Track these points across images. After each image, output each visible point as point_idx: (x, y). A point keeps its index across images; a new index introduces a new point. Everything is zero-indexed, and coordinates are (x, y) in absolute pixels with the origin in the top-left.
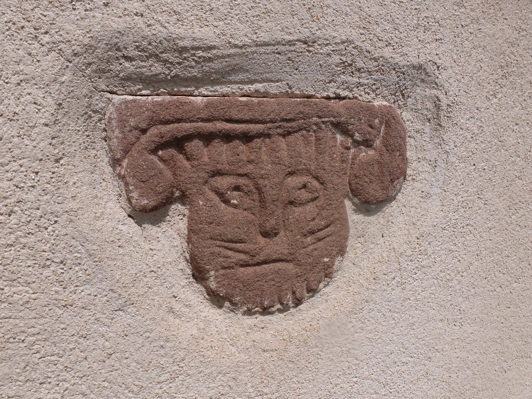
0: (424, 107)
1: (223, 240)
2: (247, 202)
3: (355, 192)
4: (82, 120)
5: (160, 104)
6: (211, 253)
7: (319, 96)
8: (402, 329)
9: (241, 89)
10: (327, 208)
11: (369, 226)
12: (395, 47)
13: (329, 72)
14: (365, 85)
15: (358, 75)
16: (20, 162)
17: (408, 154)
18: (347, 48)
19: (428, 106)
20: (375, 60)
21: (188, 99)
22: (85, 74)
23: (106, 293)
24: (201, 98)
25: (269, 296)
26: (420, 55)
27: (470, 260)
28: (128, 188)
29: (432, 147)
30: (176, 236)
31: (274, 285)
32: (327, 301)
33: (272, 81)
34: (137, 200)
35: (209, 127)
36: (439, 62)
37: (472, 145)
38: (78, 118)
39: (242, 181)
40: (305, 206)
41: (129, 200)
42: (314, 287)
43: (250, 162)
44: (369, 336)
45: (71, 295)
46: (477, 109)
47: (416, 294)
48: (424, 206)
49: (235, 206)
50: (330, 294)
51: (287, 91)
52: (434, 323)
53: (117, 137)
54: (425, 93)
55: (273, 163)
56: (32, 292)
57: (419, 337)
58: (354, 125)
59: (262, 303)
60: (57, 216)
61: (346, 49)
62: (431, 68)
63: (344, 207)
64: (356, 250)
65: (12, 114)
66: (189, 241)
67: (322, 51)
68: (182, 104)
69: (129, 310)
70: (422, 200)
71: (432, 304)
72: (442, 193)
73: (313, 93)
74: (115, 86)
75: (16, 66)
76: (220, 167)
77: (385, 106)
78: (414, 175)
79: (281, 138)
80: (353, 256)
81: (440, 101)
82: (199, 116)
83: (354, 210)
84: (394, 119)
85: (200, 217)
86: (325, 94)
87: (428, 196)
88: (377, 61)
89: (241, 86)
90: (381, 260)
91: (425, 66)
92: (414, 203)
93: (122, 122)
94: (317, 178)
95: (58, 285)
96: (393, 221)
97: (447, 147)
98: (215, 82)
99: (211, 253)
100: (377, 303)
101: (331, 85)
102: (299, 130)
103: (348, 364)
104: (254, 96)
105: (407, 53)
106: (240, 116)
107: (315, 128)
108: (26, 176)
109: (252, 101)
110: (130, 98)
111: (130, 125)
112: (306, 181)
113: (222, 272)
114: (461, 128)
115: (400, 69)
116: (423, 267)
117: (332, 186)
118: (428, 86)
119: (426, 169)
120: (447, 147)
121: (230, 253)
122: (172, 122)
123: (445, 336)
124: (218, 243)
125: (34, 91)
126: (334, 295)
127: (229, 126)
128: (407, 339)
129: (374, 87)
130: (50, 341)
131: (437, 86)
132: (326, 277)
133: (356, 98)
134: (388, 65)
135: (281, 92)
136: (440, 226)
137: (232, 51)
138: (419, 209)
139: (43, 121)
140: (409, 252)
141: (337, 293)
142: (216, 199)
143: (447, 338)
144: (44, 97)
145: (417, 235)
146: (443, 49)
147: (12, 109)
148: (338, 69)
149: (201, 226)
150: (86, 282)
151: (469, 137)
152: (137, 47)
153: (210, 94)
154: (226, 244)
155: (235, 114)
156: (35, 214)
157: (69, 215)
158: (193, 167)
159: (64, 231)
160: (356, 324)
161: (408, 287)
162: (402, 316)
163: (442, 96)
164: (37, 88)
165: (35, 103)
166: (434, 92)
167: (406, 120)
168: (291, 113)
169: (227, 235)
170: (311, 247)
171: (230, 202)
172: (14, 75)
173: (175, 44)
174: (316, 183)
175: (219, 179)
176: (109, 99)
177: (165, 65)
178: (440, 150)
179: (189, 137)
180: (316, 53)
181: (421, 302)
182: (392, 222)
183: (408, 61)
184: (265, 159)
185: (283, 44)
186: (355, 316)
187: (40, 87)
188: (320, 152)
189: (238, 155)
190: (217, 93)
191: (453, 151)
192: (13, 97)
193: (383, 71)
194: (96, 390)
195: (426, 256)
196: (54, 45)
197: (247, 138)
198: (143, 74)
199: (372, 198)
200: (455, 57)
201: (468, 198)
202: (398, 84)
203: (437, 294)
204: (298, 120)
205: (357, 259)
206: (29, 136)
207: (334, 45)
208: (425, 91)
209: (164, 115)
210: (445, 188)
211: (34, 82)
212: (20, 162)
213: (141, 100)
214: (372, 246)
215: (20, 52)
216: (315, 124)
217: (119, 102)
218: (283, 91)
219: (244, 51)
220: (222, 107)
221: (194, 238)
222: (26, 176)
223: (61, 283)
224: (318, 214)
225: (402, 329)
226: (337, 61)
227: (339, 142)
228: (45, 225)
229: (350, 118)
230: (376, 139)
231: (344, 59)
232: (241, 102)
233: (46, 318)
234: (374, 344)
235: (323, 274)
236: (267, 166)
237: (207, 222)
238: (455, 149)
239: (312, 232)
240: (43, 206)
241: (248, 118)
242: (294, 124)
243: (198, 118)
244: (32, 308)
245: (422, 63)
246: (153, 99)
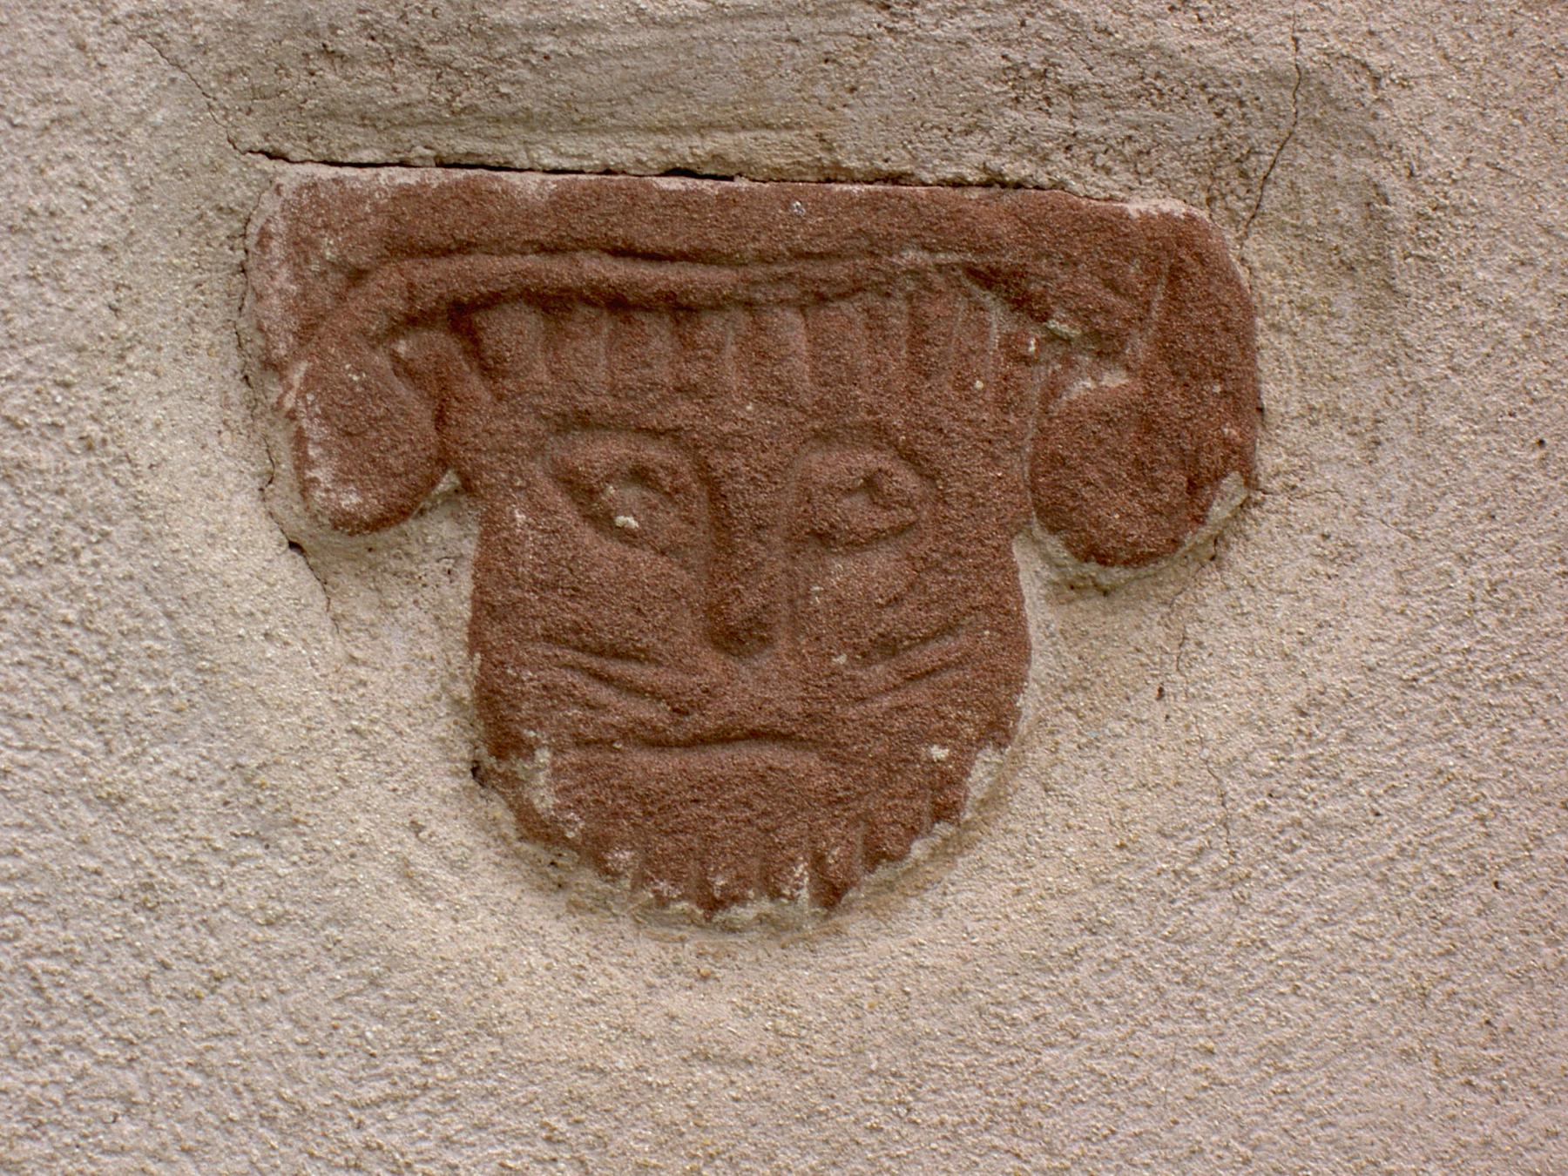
0: (1328, 221)
1: (584, 648)
2: (669, 519)
3: (1055, 517)
4: (190, 236)
5: (406, 193)
6: (545, 687)
7: (926, 176)
8: (1238, 1062)
9: (666, 152)
10: (947, 565)
11: (1109, 652)
12: (1203, 14)
13: (963, 100)
14: (1097, 141)
15: (1069, 108)
16: (29, 353)
17: (1270, 392)
18: (1029, 21)
19: (1344, 217)
20: (1132, 58)
21: (499, 180)
22: (214, 103)
23: (222, 776)
24: (539, 177)
25: (731, 859)
26: (1303, 37)
27: (1532, 823)
28: (305, 453)
29: (1364, 368)
30: (427, 626)
31: (749, 822)
32: (939, 912)
33: (768, 126)
34: (327, 491)
35: (559, 271)
36: (1376, 60)
37: (1529, 368)
38: (180, 231)
39: (655, 453)
40: (869, 554)
41: (305, 488)
42: (889, 846)
43: (686, 390)
44: (1103, 1066)
45: (125, 767)
46: (1548, 231)
47: (1294, 930)
48: (1328, 591)
49: (626, 536)
50: (952, 889)
51: (819, 160)
52: (1376, 1059)
53: (280, 291)
54: (1333, 171)
55: (763, 397)
56: (21, 744)
57: (1310, 1105)
58: (1048, 276)
59: (705, 885)
60: (108, 520)
61: (1023, 24)
62: (1345, 83)
63: (1010, 571)
64: (1058, 738)
65: (20, 215)
66: (476, 641)
67: (939, 32)
68: (475, 193)
69: (285, 842)
70: (1320, 568)
71: (1364, 981)
72: (1403, 546)
73: (907, 168)
74: (288, 137)
75: (44, 80)
76: (587, 402)
77: (1167, 217)
78: (1294, 473)
79: (791, 316)
80: (1042, 754)
81: (1387, 202)
82: (532, 236)
83: (1046, 597)
84: (1202, 262)
85: (515, 565)
86: (949, 172)
87: (1347, 554)
88: (1134, 62)
89: (665, 141)
90: (1152, 780)
91: (1324, 78)
92: (1289, 575)
93: (301, 246)
94: (909, 457)
95: (91, 732)
96: (1203, 638)
97: (1421, 373)
98: (579, 127)
99: (545, 687)
100: (1132, 941)
101: (972, 141)
102: (854, 291)
103: (1016, 1163)
104: (707, 171)
105: (1252, 31)
106: (660, 240)
107: (911, 286)
108: (38, 392)
109: (701, 192)
110: (327, 172)
111: (322, 257)
112: (873, 466)
113: (574, 756)
114: (1479, 302)
115: (1225, 85)
116: (1324, 824)
117: (965, 490)
118: (1342, 143)
119: (1341, 451)
120: (1421, 373)
121: (604, 694)
122: (447, 252)
123: (1425, 1125)
124: (570, 656)
125: (82, 151)
126: (970, 895)
127: (617, 272)
128: (1259, 1108)
129: (1128, 149)
130: (53, 907)
131: (1380, 148)
132: (937, 817)
133: (1061, 185)
134: (1179, 74)
135: (799, 163)
136: (1396, 671)
137: (645, 37)
138: (1309, 603)
139: (100, 237)
140: (1264, 761)
141: (980, 886)
142: (568, 514)
143: (1435, 1135)
144: (105, 168)
145: (1299, 697)
146: (1397, 14)
147: (23, 201)
148: (996, 89)
149: (516, 593)
150: (171, 733)
151: (1514, 336)
152: (366, 25)
153: (566, 164)
154: (596, 663)
155: (647, 235)
156: (53, 507)
157: (142, 518)
158: (500, 398)
159: (124, 568)
160: (1049, 1009)
161: (1261, 899)
162: (1237, 1007)
163: (1392, 183)
164: (89, 143)
165: (82, 186)
166: (1363, 165)
167: (1257, 265)
168: (828, 235)
169: (601, 630)
170: (886, 702)
171: (611, 519)
172: (35, 105)
173: (477, 18)
174: (906, 480)
175: (579, 438)
176: (264, 173)
177: (439, 76)
178: (1393, 382)
179: (493, 300)
180: (918, 38)
181: (1316, 966)
182: (1199, 644)
183: (1255, 61)
184: (750, 383)
185: (808, 14)
186: (1044, 980)
187: (99, 140)
188: (921, 369)
189: (649, 366)
190: (586, 163)
191: (1446, 388)
192: (27, 167)
193: (1161, 94)
194: (166, 1093)
195: (1335, 786)
196: (147, 23)
197: (680, 309)
198: (371, 100)
199: (1112, 543)
200: (1447, 41)
201: (1517, 573)
202: (1222, 136)
203: (1384, 943)
204: (852, 257)
205: (1059, 770)
206: (59, 278)
207: (980, 13)
208: (1332, 164)
209: (427, 230)
210: (1416, 528)
211: (84, 124)
212: (29, 353)
213: (356, 179)
214: (1118, 727)
215: (56, 41)
216: (908, 272)
217: (295, 184)
218: (806, 159)
219: (685, 36)
220: (604, 208)
221: (493, 634)
222: (38, 392)
223: (101, 728)
224: (911, 586)
225: (1238, 1062)
226: (991, 63)
227: (995, 339)
228: (75, 544)
229: (1037, 257)
230: (1134, 331)
231: (1018, 57)
232: (664, 194)
233: (51, 831)
234: (1121, 1103)
235: (926, 806)
236: (742, 407)
237: (536, 581)
238: (1455, 380)
239: (888, 646)
240: (76, 486)
241: (685, 247)
242: (839, 271)
243: (528, 242)
244: (16, 795)
245: (1309, 65)
246: (391, 178)
